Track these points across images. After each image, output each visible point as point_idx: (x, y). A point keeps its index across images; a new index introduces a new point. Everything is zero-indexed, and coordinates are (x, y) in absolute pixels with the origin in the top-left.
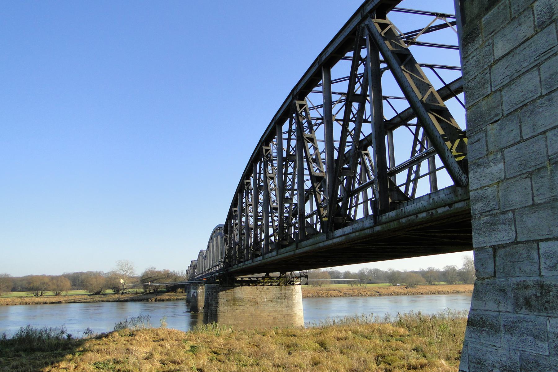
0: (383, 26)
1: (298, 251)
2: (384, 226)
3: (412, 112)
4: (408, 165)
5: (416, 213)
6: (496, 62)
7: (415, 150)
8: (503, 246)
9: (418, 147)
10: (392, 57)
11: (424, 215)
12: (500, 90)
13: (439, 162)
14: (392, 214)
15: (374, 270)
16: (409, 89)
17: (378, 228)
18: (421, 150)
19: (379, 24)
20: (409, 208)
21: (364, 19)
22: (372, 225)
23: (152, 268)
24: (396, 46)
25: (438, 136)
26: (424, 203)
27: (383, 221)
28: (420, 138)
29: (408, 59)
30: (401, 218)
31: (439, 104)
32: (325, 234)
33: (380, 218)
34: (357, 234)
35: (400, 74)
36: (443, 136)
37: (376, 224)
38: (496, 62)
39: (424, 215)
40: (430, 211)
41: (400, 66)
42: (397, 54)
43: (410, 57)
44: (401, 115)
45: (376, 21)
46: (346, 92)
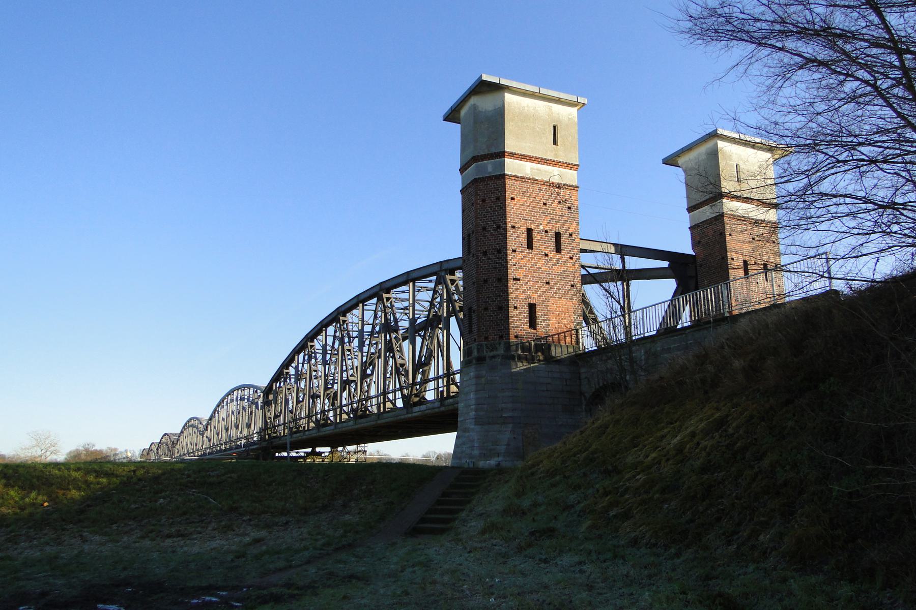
1: (379, 422)
2: (446, 407)
15: (445, 455)
17: (442, 409)
19: (451, 280)
22: (439, 406)
23: (88, 445)
27: (446, 404)
32: (406, 410)
34: (430, 411)
37: (442, 405)
46: (370, 330)
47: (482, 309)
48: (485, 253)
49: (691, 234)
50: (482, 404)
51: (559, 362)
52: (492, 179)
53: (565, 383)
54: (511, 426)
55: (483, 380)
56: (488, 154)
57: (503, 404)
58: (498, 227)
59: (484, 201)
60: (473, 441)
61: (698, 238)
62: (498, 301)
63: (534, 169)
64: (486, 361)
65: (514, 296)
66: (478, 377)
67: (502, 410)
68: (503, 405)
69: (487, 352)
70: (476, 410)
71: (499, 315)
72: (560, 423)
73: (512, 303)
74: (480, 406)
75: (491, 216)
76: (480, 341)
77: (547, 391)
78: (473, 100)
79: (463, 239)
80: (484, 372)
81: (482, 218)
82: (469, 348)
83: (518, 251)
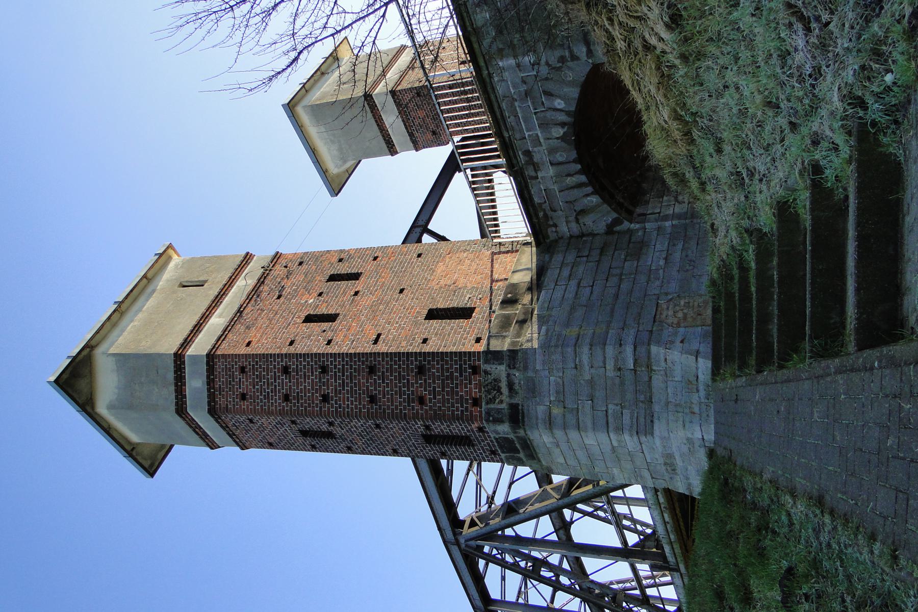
0: (473, 524)
2: (679, 560)
3: (555, 513)
4: (620, 529)
5: (665, 523)
6: (566, 463)
7: (605, 518)
8: (651, 474)
9: (601, 514)
10: (508, 519)
11: (666, 515)
12: (580, 464)
13: (619, 493)
14: (667, 549)
16: (544, 509)
18: (605, 511)
19: (470, 527)
20: (661, 530)
21: (457, 543)
24: (497, 515)
25: (593, 490)
26: (656, 513)
27: (674, 560)
28: (590, 509)
29: (513, 505)
30: (670, 539)
31: (564, 486)
33: (672, 564)
35: (527, 515)
36: (594, 486)
37: (677, 570)
38: (566, 463)
39: (666, 515)
40: (663, 509)
41: (519, 513)
42: (506, 515)
43: (512, 503)
44: (557, 527)
45: (466, 531)
47: (422, 409)
48: (325, 398)
49: (424, 148)
50: (607, 416)
51: (541, 271)
52: (213, 379)
53: (585, 259)
54: (654, 349)
55: (556, 411)
56: (176, 385)
57: (608, 367)
58: (286, 370)
59: (243, 397)
60: (690, 441)
61: (430, 136)
62: (408, 375)
63: (222, 313)
64: (518, 404)
65: (404, 344)
66: (550, 423)
67: (619, 369)
68: (610, 365)
69: (501, 402)
70: (620, 429)
71: (434, 373)
72: (662, 263)
73: (416, 347)
74: (611, 420)
75: (268, 384)
76: (481, 416)
77: (592, 286)
78: (102, 409)
79: (314, 448)
80: (541, 409)
81: (269, 402)
82: (501, 447)
83: (333, 336)
